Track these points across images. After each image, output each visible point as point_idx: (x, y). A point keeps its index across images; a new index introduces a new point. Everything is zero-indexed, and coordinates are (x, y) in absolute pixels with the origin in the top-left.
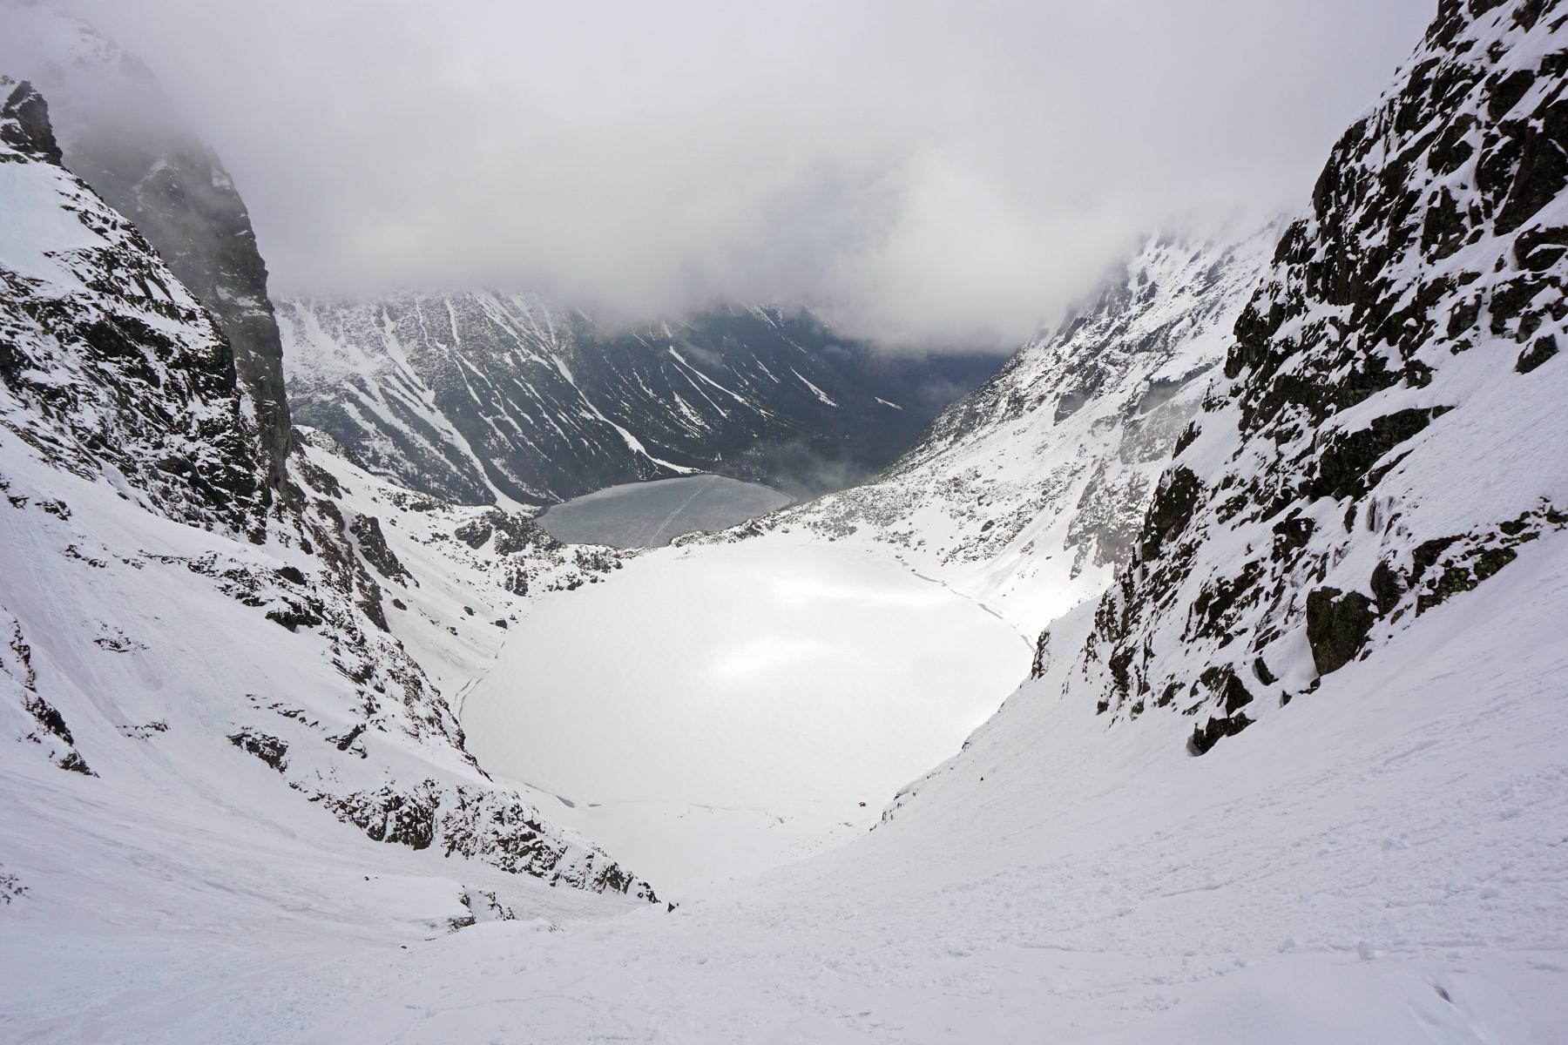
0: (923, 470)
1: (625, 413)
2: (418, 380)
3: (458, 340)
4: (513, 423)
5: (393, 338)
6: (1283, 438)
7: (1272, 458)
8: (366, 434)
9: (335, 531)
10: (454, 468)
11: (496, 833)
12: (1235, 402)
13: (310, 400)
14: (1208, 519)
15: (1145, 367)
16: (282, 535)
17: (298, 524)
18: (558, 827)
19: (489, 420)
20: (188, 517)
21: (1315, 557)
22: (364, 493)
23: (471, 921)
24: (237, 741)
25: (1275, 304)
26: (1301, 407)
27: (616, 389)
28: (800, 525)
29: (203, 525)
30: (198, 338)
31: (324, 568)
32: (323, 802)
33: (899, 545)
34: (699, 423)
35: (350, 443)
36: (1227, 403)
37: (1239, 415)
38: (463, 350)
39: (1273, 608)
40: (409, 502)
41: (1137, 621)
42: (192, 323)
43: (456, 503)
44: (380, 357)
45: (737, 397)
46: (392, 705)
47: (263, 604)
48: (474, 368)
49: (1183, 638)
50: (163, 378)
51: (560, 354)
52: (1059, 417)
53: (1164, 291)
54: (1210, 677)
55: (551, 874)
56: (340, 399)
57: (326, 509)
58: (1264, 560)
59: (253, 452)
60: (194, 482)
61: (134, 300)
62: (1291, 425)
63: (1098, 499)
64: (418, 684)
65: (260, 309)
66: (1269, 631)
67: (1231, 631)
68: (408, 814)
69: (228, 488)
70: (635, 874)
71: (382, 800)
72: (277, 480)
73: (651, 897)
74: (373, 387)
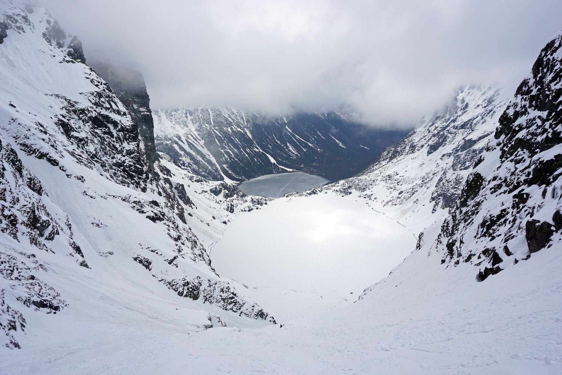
1: (270, 149)
2: (198, 137)
3: (213, 123)
5: (191, 122)
6: (517, 162)
7: (513, 170)
8: (181, 155)
10: (210, 168)
12: (498, 148)
13: (162, 143)
14: (486, 192)
15: (463, 135)
16: (152, 189)
17: (157, 186)
18: (243, 295)
19: (222, 151)
20: (122, 182)
21: (530, 208)
23: (212, 326)
24: (135, 259)
26: (525, 150)
27: (267, 141)
29: (126, 185)
34: (296, 153)
35: (175, 159)
36: (495, 149)
37: (500, 153)
38: (214, 126)
39: (512, 227)
40: (195, 179)
44: (186, 128)
45: (309, 144)
46: (187, 249)
48: (218, 133)
49: (475, 237)
50: (115, 135)
51: (248, 128)
52: (429, 153)
53: (471, 106)
54: (486, 252)
55: (239, 312)
56: (172, 143)
57: (167, 181)
58: (509, 208)
59: (143, 161)
60: (124, 170)
61: (107, 109)
62: (521, 157)
63: (443, 184)
64: (196, 243)
67: (495, 235)
68: (191, 288)
69: (135, 173)
71: (182, 282)
72: (151, 170)
73: (274, 322)
74: (183, 139)
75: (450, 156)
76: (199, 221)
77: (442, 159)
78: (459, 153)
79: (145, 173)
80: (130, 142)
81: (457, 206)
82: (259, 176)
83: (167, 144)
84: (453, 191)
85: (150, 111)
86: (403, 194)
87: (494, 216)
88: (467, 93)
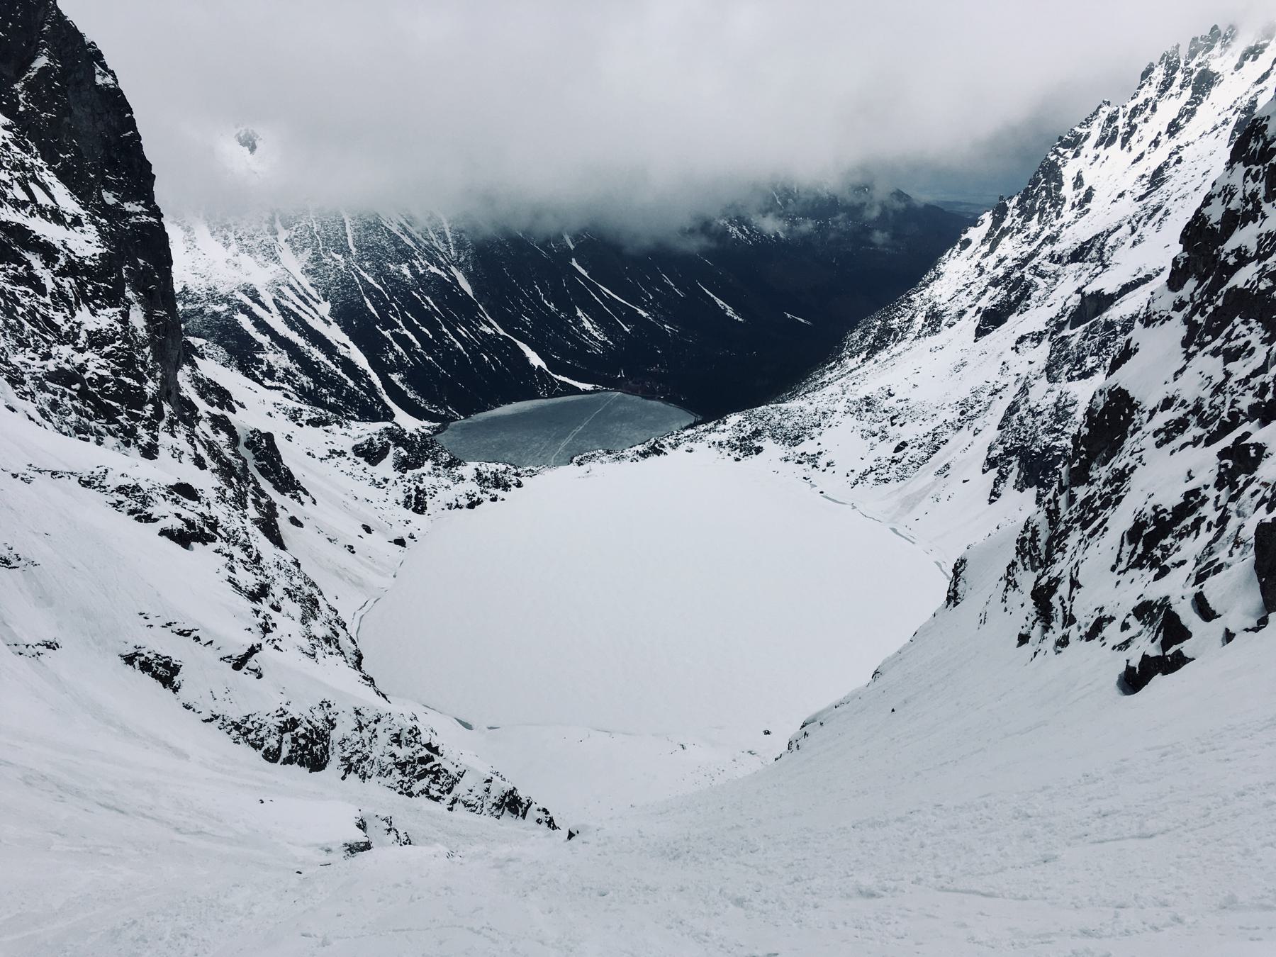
0: (834, 388)
1: (526, 327)
2: (312, 291)
3: (354, 250)
4: (412, 337)
5: (287, 246)
6: (1231, 356)
7: (1218, 378)
8: (260, 346)
9: (229, 446)
10: (351, 383)
11: (393, 755)
12: (1178, 317)
13: (201, 311)
14: (1144, 443)
15: (1076, 278)
16: (174, 450)
17: (191, 438)
18: (457, 751)
19: (387, 333)
20: (77, 430)
21: (1266, 485)
22: (259, 407)
23: (367, 846)
24: (129, 660)
25: (1228, 210)
26: (1253, 323)
28: (705, 444)
29: (93, 439)
30: (85, 243)
31: (218, 485)
32: (217, 723)
33: (807, 466)
34: (602, 338)
35: (243, 354)
36: (1169, 318)
37: (1183, 331)
38: (360, 260)
39: (1215, 539)
40: (305, 417)
41: (1063, 550)
42: (78, 229)
43: (353, 418)
44: (273, 266)
45: (641, 312)
46: (288, 623)
47: (156, 520)
48: (371, 280)
49: (1113, 569)
50: (50, 286)
51: (459, 266)
52: (980, 333)
54: (1144, 611)
57: (220, 423)
58: (1206, 487)
59: (144, 364)
60: (84, 394)
61: (18, 205)
62: (1241, 342)
63: (1021, 419)
64: (315, 603)
65: (148, 215)
66: (1212, 563)
67: (1168, 562)
68: (304, 736)
69: (112, 404)
70: (533, 799)
71: (277, 721)
72: (169, 393)
73: (551, 823)
74: (267, 298)
75: (1039, 341)
76: (323, 538)
77: (1017, 349)
78: (1067, 332)
79: (152, 401)
80: (99, 307)
81: (1060, 482)
82: (497, 406)
83: (216, 314)
84: (1047, 439)
85: (157, 213)
86: (907, 449)
87: (1165, 511)
88: (1091, 159)
